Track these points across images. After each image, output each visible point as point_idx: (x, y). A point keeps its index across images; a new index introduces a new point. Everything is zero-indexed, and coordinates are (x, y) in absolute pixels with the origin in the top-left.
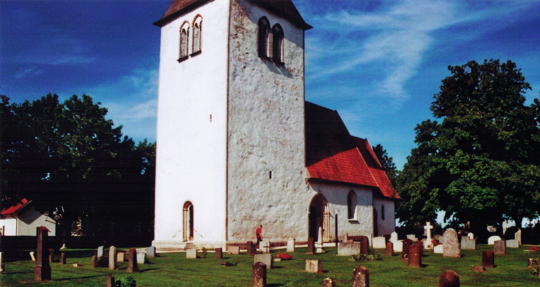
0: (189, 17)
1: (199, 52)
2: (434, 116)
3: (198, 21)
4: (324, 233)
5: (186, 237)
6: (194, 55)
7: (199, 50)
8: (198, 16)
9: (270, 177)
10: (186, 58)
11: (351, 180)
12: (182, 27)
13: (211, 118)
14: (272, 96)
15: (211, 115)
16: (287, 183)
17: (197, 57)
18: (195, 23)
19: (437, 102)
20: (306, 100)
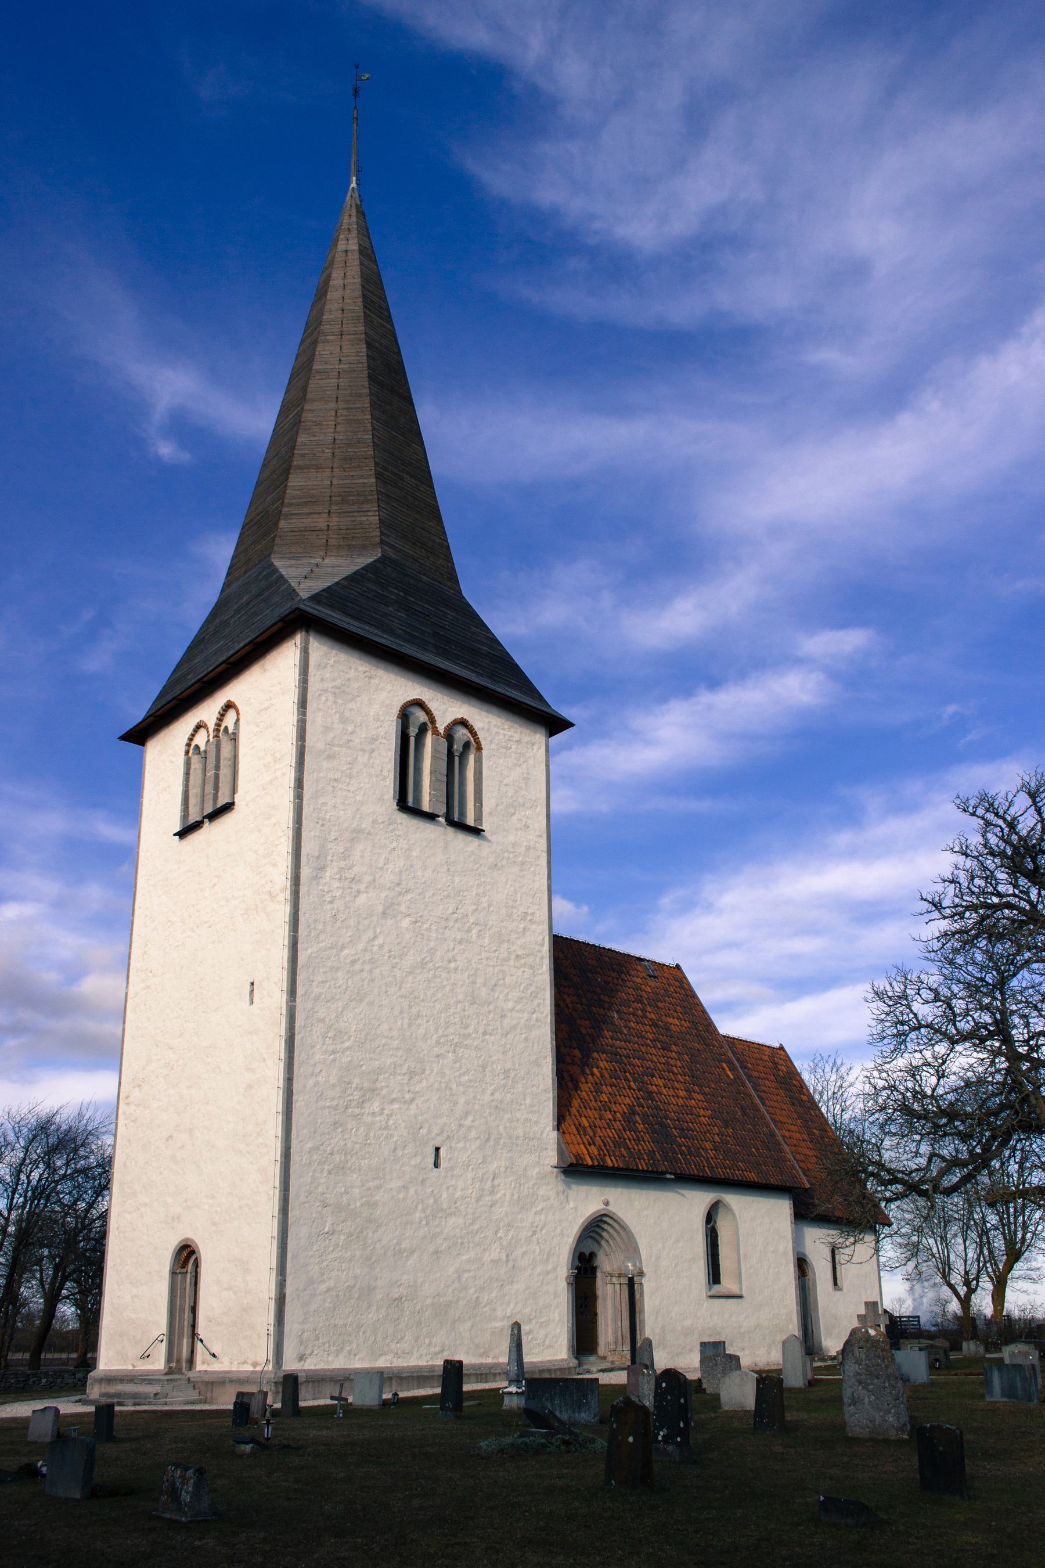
0: (207, 711)
1: (228, 807)
2: (484, 831)
3: (229, 720)
4: (192, 1304)
5: (179, 1361)
6: (214, 815)
7: (227, 800)
8: (229, 706)
9: (436, 1165)
10: (196, 826)
11: (711, 1168)
12: (191, 740)
13: (252, 991)
14: (443, 924)
15: (252, 984)
16: (106, 1132)
17: (227, 821)
18: (222, 728)
19: (967, 939)
20: (556, 932)
